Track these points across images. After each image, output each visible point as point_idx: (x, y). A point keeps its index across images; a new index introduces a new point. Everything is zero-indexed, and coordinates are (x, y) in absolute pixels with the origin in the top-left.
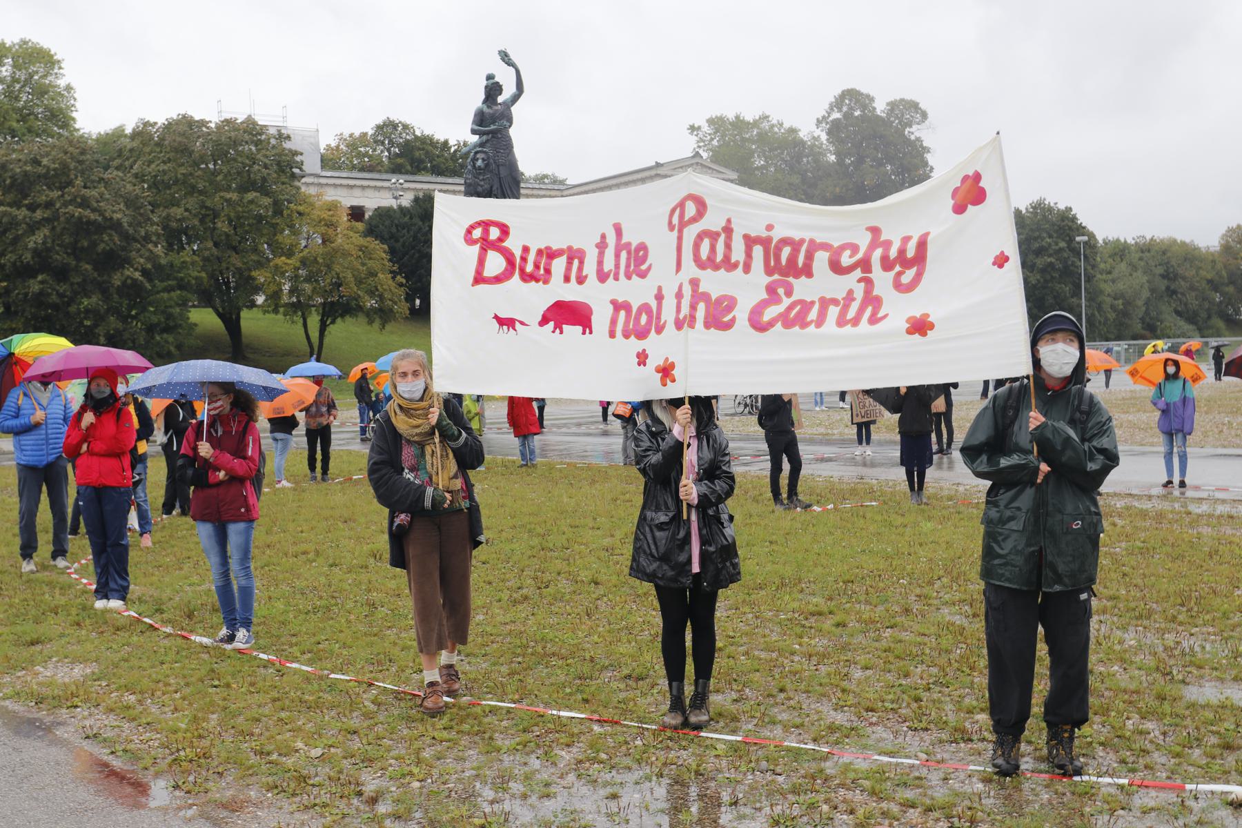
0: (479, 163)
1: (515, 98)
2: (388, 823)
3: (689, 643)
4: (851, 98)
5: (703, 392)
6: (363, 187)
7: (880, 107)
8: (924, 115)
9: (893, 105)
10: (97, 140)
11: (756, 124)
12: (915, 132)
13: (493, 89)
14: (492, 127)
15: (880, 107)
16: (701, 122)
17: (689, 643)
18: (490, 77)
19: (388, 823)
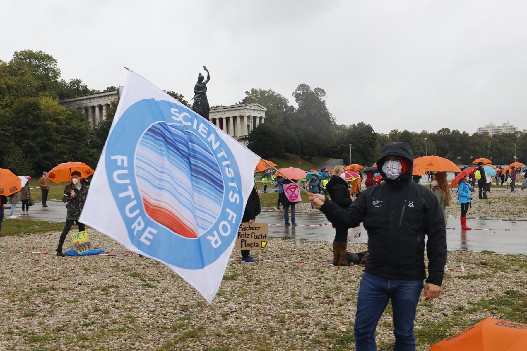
0: (199, 103)
1: (207, 81)
2: (305, 350)
3: (427, 263)
4: (303, 87)
5: (442, 170)
6: (218, 112)
7: (312, 89)
8: (325, 93)
9: (316, 89)
10: (495, 136)
11: (268, 92)
12: (322, 99)
13: (201, 78)
14: (202, 91)
15: (312, 89)
16: (250, 91)
17: (427, 263)
18: (200, 74)
19: (305, 350)
